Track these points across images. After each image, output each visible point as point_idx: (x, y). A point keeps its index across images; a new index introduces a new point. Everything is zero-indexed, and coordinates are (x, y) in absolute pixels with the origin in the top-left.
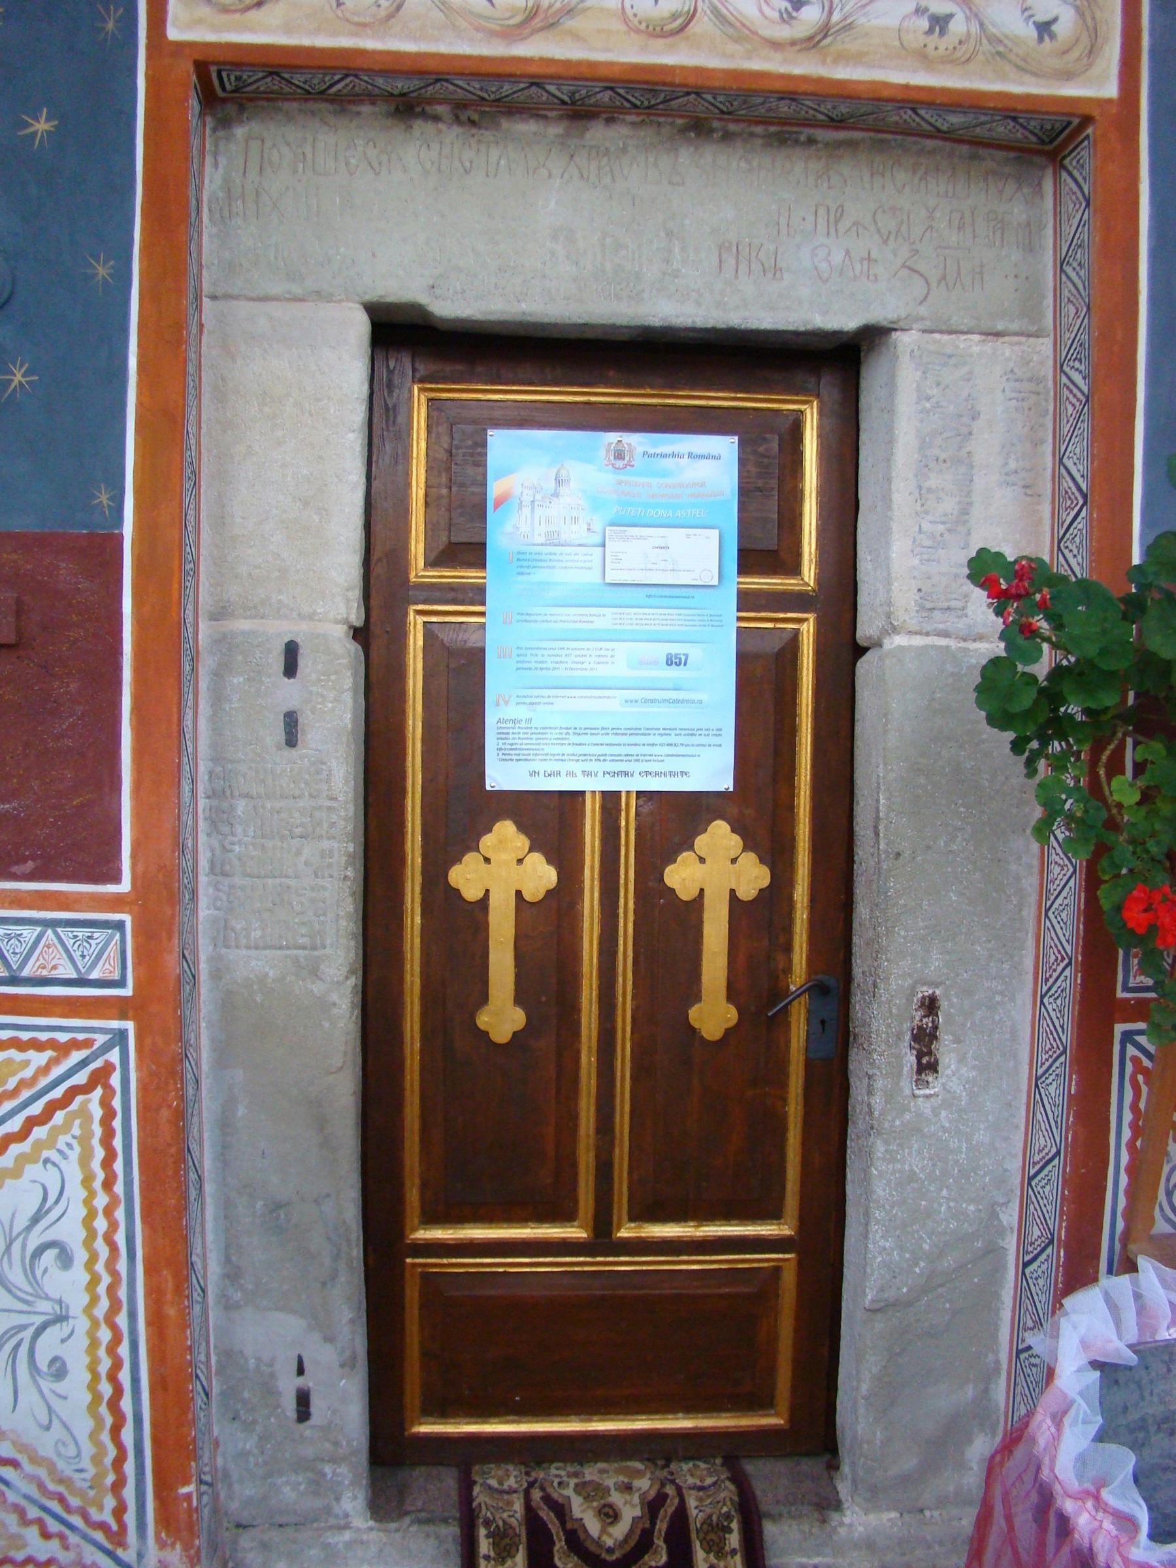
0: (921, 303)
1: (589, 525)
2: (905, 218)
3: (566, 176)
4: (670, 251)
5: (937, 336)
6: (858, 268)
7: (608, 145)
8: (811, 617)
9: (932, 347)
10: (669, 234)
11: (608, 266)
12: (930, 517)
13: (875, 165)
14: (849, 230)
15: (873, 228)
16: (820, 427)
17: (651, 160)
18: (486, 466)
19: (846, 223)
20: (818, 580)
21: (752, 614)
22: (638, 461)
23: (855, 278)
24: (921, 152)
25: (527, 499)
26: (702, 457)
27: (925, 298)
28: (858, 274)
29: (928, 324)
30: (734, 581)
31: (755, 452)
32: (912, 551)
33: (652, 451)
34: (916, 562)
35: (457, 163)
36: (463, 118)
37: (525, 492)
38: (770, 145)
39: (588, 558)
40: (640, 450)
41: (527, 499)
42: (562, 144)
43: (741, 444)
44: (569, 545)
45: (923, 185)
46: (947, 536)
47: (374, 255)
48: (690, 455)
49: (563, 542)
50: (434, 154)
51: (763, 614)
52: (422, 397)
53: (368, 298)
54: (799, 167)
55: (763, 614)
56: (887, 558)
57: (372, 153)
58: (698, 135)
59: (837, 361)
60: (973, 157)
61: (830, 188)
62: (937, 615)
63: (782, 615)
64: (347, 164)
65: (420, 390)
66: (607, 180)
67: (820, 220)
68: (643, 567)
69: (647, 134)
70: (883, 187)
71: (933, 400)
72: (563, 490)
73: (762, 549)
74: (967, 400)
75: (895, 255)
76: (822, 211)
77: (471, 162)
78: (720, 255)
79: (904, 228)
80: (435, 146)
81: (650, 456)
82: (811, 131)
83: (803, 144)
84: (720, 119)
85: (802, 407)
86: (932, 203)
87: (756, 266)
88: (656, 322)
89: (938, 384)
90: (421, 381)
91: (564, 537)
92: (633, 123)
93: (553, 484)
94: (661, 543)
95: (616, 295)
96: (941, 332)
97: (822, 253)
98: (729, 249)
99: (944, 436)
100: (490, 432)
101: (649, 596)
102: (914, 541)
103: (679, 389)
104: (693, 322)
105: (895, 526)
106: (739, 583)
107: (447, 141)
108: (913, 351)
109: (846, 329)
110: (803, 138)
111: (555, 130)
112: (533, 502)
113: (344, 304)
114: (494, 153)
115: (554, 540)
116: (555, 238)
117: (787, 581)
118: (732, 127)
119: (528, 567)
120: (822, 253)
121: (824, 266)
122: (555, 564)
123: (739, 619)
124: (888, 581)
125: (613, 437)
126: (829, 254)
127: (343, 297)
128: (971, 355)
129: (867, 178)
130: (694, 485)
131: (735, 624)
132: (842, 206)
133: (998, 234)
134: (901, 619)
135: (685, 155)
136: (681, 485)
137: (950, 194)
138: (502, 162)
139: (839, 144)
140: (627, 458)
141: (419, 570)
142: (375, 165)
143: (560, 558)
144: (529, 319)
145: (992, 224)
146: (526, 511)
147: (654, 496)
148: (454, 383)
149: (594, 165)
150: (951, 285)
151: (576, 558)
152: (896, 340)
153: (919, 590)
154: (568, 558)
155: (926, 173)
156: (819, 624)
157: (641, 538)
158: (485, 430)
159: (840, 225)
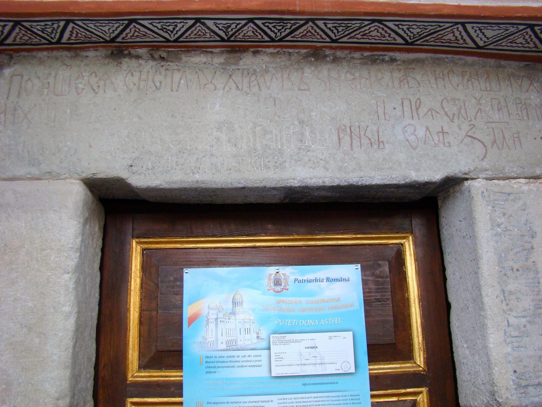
0: (482, 160)
1: (258, 333)
2: (462, 104)
3: (227, 88)
4: (303, 134)
5: (495, 181)
6: (436, 139)
7: (255, 67)
8: (424, 390)
9: (496, 189)
10: (301, 122)
11: (258, 146)
12: (514, 314)
13: (437, 73)
14: (426, 114)
15: (442, 112)
16: (416, 254)
17: (285, 76)
18: (182, 294)
19: (423, 110)
20: (428, 361)
21: (381, 392)
22: (292, 286)
23: (436, 145)
24: (465, 64)
25: (212, 317)
26: (336, 280)
27: (485, 156)
28: (437, 142)
29: (489, 174)
30: (366, 369)
31: (373, 275)
32: (505, 341)
33: (300, 278)
34: (509, 350)
35: (151, 84)
36: (156, 56)
37: (211, 312)
38: (366, 64)
39: (259, 358)
40: (292, 278)
41: (212, 317)
42: (224, 69)
43: (363, 269)
44: (243, 350)
45: (469, 83)
46: (529, 326)
47: (90, 146)
48: (328, 279)
49: (239, 347)
50: (136, 79)
51: (389, 391)
52: (139, 247)
53: (84, 175)
54: (387, 76)
55: (389, 391)
56: (485, 347)
57: (93, 80)
58: (317, 60)
59: (422, 206)
60: (499, 66)
61: (410, 88)
62: (531, 389)
63: (403, 391)
64: (77, 88)
65: (137, 243)
66: (255, 89)
67: (406, 109)
68: (299, 362)
69: (282, 60)
70: (445, 86)
71: (503, 226)
72: (238, 309)
73: (384, 342)
74: (526, 224)
75: (460, 129)
76: (406, 103)
77: (161, 82)
78: (339, 136)
79: (463, 111)
80: (137, 74)
81: (300, 282)
82: (391, 54)
83: (387, 61)
84: (331, 48)
85: (402, 241)
86: (478, 95)
87: (365, 141)
88: (295, 183)
89: (504, 214)
90: (138, 237)
91: (240, 344)
92: (271, 53)
93: (230, 306)
94: (311, 344)
95: (265, 165)
96: (498, 179)
97: (410, 130)
98: (344, 130)
99: (515, 251)
100: (185, 270)
101: (305, 384)
102: (505, 333)
103: (317, 235)
104: (323, 182)
105: (489, 323)
106: (370, 370)
107: (145, 70)
108: (483, 192)
109: (434, 180)
110: (387, 58)
111: (218, 60)
112: (217, 319)
113: (68, 180)
114: (177, 76)
115: (232, 346)
116: (219, 129)
117: (404, 365)
118: (339, 53)
119: (214, 367)
120: (410, 130)
121: (412, 138)
122: (233, 364)
123: (372, 396)
124: (489, 366)
125: (272, 270)
126: (415, 130)
127: (67, 175)
128: (523, 193)
129: (433, 81)
130: (332, 300)
131: (369, 401)
132: (419, 99)
133: (524, 112)
134: (504, 397)
135: (309, 72)
136: (323, 301)
137: (488, 89)
138: (182, 81)
139: (413, 61)
140: (283, 284)
141: (135, 373)
142: (95, 88)
143: (238, 359)
144: (202, 186)
145: (519, 106)
146: (212, 326)
147: (304, 310)
148: (161, 237)
149: (246, 80)
150: (500, 146)
151: (249, 359)
152: (469, 187)
153: (515, 372)
154: (244, 359)
155: (470, 76)
156: (430, 394)
157: (296, 341)
158: (183, 269)
159: (420, 110)
